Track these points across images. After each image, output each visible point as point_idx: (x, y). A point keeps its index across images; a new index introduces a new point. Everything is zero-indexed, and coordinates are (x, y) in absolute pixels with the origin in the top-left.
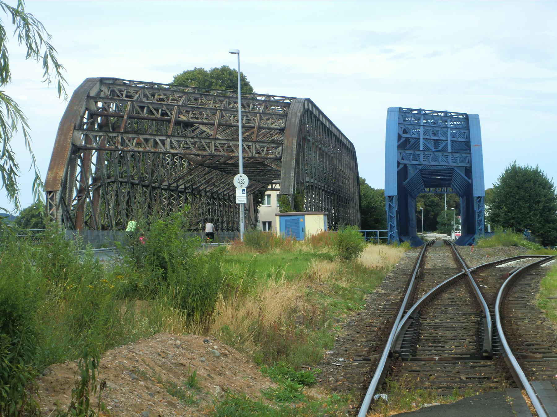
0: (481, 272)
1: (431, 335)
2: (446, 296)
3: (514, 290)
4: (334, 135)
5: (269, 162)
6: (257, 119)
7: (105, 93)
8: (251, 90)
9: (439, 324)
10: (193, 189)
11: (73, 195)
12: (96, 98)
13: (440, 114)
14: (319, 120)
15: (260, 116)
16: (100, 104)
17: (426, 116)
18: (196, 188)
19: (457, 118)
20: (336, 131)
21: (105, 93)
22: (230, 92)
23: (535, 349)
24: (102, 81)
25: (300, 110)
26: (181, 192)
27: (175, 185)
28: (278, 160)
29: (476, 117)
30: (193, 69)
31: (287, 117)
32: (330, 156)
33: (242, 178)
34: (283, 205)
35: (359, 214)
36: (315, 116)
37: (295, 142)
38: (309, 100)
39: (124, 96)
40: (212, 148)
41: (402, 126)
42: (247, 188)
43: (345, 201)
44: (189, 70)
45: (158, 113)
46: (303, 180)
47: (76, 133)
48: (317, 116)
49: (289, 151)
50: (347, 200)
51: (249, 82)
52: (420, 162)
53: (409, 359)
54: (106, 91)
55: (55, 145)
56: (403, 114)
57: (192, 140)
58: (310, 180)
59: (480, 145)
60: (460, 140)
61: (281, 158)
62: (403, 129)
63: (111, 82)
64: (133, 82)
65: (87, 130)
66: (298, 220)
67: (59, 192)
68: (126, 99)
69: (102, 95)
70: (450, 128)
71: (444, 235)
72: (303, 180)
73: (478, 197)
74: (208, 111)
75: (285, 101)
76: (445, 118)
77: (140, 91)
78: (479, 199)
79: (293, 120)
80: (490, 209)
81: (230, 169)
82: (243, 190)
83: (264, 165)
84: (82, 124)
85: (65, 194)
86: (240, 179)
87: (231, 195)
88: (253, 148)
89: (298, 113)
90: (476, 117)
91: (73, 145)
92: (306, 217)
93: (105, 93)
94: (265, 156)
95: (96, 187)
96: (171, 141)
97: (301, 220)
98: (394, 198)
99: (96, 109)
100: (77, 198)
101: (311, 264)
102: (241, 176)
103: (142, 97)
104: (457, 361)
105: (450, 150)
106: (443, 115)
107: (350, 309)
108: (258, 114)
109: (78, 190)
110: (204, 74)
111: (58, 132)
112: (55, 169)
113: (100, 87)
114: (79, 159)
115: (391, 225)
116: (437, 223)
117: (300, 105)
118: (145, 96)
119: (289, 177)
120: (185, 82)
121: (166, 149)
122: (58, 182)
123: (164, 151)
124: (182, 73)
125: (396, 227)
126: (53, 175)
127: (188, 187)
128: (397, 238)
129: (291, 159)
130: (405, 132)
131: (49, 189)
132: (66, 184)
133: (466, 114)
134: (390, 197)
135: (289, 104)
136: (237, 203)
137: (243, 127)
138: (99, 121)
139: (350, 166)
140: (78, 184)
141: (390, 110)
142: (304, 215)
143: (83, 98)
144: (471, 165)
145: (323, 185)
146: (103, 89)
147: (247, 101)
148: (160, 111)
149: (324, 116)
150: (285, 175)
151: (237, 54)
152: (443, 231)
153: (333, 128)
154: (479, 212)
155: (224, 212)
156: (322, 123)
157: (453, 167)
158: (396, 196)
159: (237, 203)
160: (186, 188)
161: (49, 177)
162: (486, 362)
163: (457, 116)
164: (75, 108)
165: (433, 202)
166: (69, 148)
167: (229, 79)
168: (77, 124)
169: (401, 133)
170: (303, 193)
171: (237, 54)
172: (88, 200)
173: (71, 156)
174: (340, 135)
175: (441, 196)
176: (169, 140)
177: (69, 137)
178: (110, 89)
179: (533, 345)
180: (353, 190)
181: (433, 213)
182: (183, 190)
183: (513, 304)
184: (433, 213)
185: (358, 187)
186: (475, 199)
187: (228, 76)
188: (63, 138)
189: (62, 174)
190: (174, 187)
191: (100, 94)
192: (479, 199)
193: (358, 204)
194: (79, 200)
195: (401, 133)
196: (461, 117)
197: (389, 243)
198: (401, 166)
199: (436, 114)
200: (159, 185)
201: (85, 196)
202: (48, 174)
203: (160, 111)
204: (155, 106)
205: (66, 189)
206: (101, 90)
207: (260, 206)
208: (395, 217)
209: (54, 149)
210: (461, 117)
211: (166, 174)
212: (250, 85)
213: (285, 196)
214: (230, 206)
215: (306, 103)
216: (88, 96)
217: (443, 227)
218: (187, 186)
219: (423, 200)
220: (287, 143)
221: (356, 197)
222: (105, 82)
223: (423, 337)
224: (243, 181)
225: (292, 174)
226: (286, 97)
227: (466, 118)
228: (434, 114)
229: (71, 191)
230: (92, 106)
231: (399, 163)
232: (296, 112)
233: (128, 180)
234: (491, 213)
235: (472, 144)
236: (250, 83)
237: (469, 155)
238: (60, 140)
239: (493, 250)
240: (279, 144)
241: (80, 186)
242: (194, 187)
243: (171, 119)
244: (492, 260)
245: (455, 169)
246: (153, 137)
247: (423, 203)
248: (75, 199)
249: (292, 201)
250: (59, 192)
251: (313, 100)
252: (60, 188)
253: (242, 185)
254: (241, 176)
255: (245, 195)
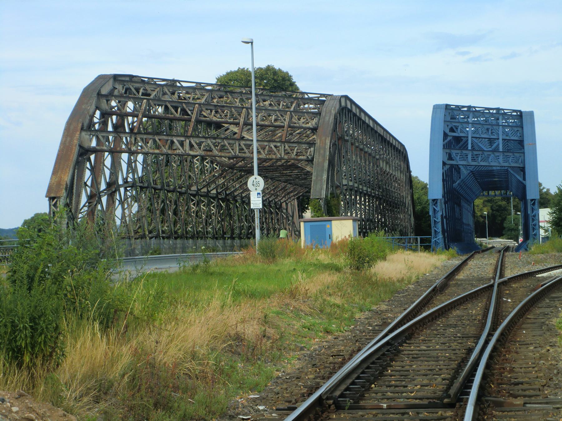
0: (515, 283)
1: (403, 369)
2: (456, 313)
3: (540, 305)
4: (380, 135)
5: (303, 164)
6: (287, 118)
7: (119, 91)
8: (297, 89)
9: (423, 352)
10: (227, 195)
11: (80, 201)
12: (109, 96)
13: (491, 111)
14: (360, 119)
15: (291, 114)
16: (113, 103)
17: (476, 113)
18: (229, 194)
19: (511, 115)
20: (382, 131)
21: (119, 91)
22: (259, 89)
23: (522, 390)
24: (116, 78)
25: (335, 108)
26: (213, 198)
27: (205, 190)
28: (310, 161)
29: (531, 114)
30: (236, 69)
31: (320, 115)
32: (374, 157)
33: (257, 180)
34: (314, 210)
35: (412, 219)
36: (355, 115)
37: (328, 142)
38: (346, 97)
39: (140, 94)
40: (236, 150)
41: (449, 124)
42: (263, 191)
43: (395, 206)
44: (233, 70)
45: (177, 111)
46: (340, 184)
47: (83, 133)
48: (358, 114)
49: (322, 152)
50: (396, 205)
51: (295, 82)
52: (468, 162)
53: (347, 408)
54: (120, 89)
55: (60, 147)
56: (450, 111)
57: (214, 141)
58: (348, 182)
59: (534, 144)
60: (513, 138)
61: (313, 158)
62: (449, 127)
63: (127, 79)
64: (153, 79)
65: (100, 130)
66: (325, 225)
67: (63, 198)
68: (142, 97)
69: (116, 92)
70: (503, 126)
71: (510, 241)
72: (340, 184)
73: (532, 200)
74: (233, 109)
75: (320, 99)
76: (497, 116)
77: (159, 89)
78: (533, 201)
79: (327, 118)
80: (554, 213)
81: (264, 172)
82: (258, 194)
83: (298, 167)
84: (91, 124)
85: (71, 200)
86: (255, 182)
87: (272, 201)
88: (282, 149)
89: (332, 111)
90: (531, 114)
91: (81, 147)
92: (333, 222)
93: (119, 90)
94: (295, 157)
95: (110, 192)
96: (190, 142)
97: (328, 226)
98: (439, 201)
99: (107, 108)
100: (87, 204)
101: (298, 277)
102: (256, 179)
103: (161, 95)
104: (407, 411)
105: (501, 149)
106: (495, 112)
107: (328, 332)
108: (289, 113)
109: (88, 196)
110: (247, 74)
111: (64, 133)
112: (59, 173)
113: (114, 84)
114: (88, 163)
115: (435, 231)
116: (504, 228)
117: (336, 102)
118: (164, 94)
119: (321, 180)
120: (228, 83)
121: (185, 151)
122: (62, 187)
123: (182, 153)
124: (225, 73)
125: (441, 232)
126: (57, 179)
127: (221, 192)
128: (442, 244)
129: (324, 161)
130: (452, 130)
131: (53, 195)
132: (72, 189)
133: (520, 111)
134: (434, 200)
135: (324, 101)
136: (252, 208)
137: (257, 125)
138: (114, 121)
139: (401, 168)
140: (88, 190)
141: (436, 108)
142: (331, 221)
143: (93, 96)
144: (524, 165)
145: (365, 188)
146: (117, 86)
147: (278, 98)
148: (179, 110)
149: (366, 114)
150: (317, 178)
151: (250, 44)
152: (509, 237)
153: (379, 127)
154: (533, 216)
155: (264, 219)
156: (364, 122)
157: (506, 168)
158: (441, 200)
159: (252, 208)
160: (218, 193)
161: (53, 182)
162: (445, 412)
163: (510, 114)
164: (83, 107)
165: (500, 206)
166: (75, 150)
167: (273, 79)
168: (86, 124)
169: (447, 131)
170: (338, 197)
171: (250, 44)
172: (99, 207)
173: (77, 159)
174: (388, 135)
175: (508, 200)
176: (188, 141)
177: (75, 138)
178: (125, 87)
179: (522, 383)
180: (405, 193)
181: (500, 218)
182: (215, 195)
183: (528, 323)
184: (500, 218)
185: (411, 191)
186: (529, 201)
187: (272, 76)
188: (69, 139)
189: (67, 178)
190: (204, 192)
191: (113, 92)
192: (533, 201)
193: (411, 208)
194: (89, 207)
195: (447, 131)
196: (515, 114)
197: (433, 251)
198: (447, 167)
199: (487, 111)
200: (186, 191)
201: (96, 202)
202: (51, 178)
203: (179, 110)
204: (174, 104)
205: (73, 195)
206: (114, 88)
207: (306, 212)
208: (440, 222)
209: (59, 151)
210: (515, 114)
211: (194, 179)
212: (296, 85)
213: (316, 200)
214: (272, 213)
215: (343, 100)
216: (99, 95)
217: (509, 233)
218: (219, 191)
219: (490, 204)
220: (320, 143)
221: (408, 200)
222: (120, 79)
223: (391, 371)
224: (258, 183)
225: (325, 177)
226: (321, 94)
227: (520, 115)
228: (485, 111)
229: (79, 196)
230: (103, 105)
231: (444, 164)
232: (331, 109)
233: (148, 185)
234: (555, 217)
235: (526, 143)
236: (296, 83)
237: (522, 155)
238: (65, 141)
239: (545, 256)
240: (311, 144)
241: (91, 191)
242: (227, 192)
243: (191, 118)
244: (535, 269)
245: (509, 170)
246: (170, 138)
247: (489, 208)
248: (84, 206)
249: (324, 206)
250: (63, 198)
251: (351, 96)
252: (63, 193)
253: (257, 188)
254: (256, 179)
255: (261, 199)
